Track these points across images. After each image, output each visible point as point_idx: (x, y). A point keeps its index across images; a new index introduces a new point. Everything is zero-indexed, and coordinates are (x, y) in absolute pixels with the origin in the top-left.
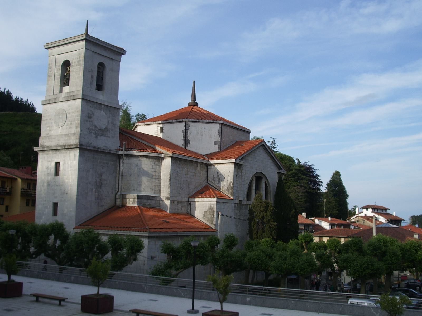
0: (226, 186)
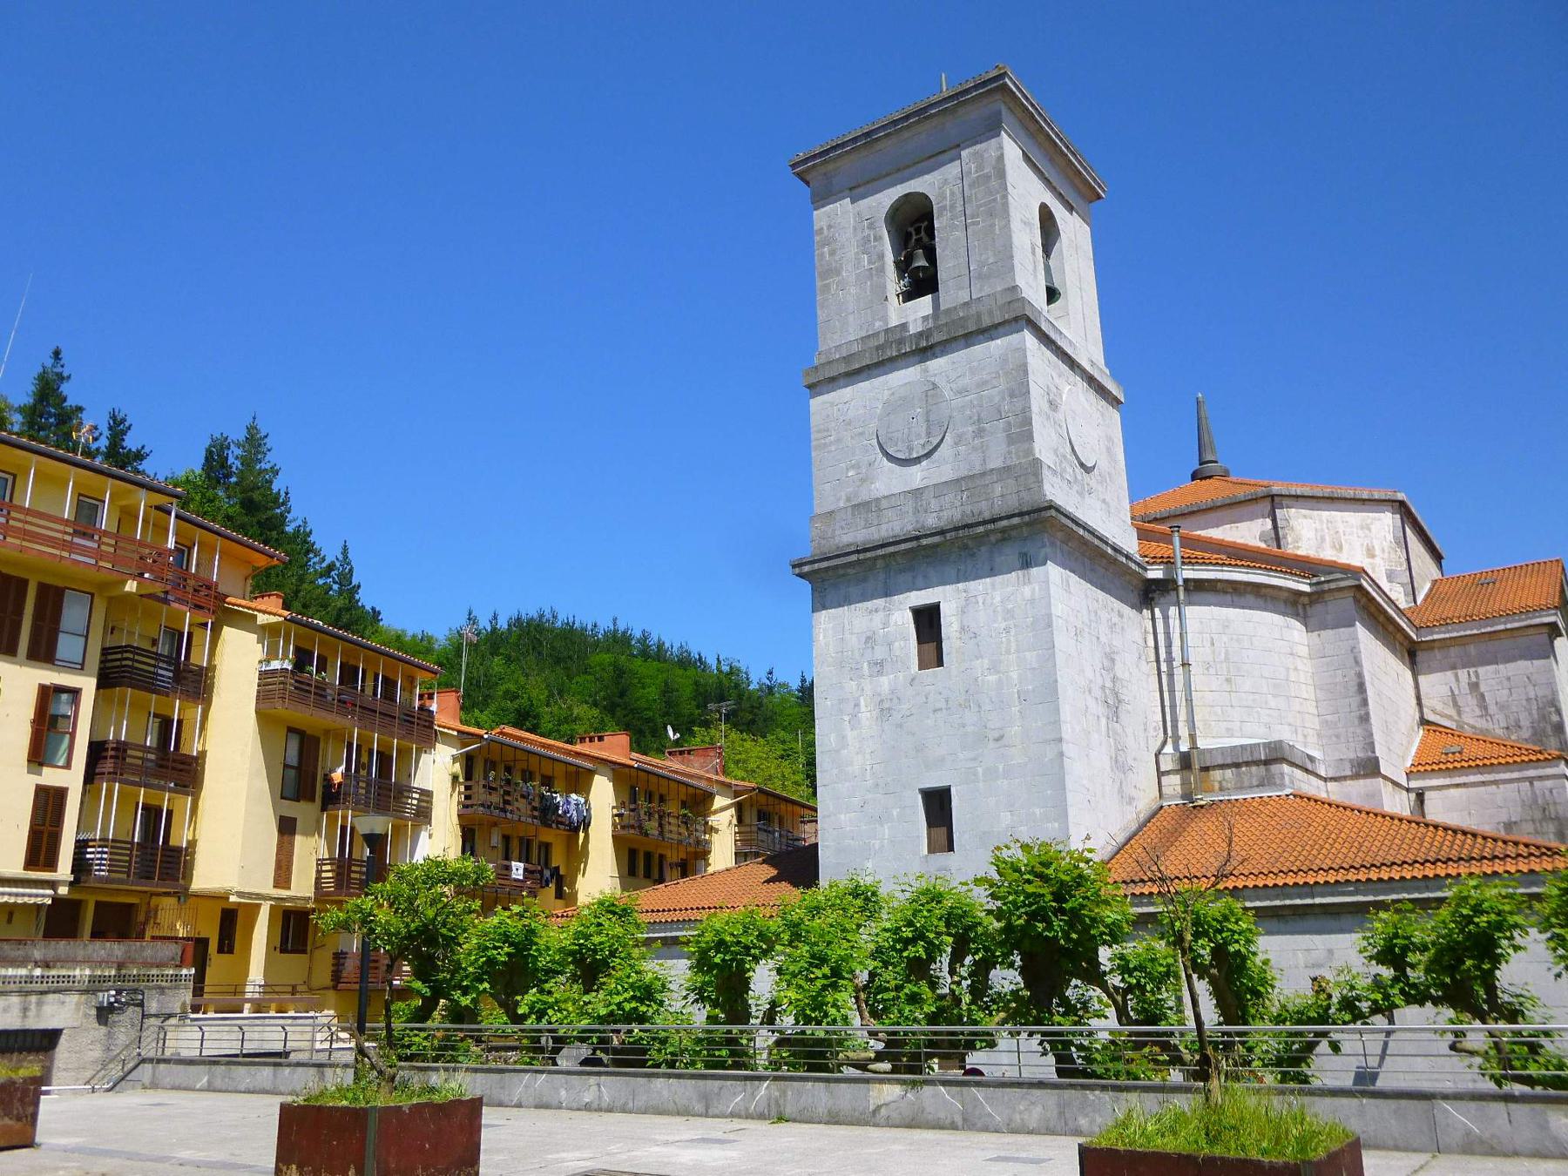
0: (1525, 723)
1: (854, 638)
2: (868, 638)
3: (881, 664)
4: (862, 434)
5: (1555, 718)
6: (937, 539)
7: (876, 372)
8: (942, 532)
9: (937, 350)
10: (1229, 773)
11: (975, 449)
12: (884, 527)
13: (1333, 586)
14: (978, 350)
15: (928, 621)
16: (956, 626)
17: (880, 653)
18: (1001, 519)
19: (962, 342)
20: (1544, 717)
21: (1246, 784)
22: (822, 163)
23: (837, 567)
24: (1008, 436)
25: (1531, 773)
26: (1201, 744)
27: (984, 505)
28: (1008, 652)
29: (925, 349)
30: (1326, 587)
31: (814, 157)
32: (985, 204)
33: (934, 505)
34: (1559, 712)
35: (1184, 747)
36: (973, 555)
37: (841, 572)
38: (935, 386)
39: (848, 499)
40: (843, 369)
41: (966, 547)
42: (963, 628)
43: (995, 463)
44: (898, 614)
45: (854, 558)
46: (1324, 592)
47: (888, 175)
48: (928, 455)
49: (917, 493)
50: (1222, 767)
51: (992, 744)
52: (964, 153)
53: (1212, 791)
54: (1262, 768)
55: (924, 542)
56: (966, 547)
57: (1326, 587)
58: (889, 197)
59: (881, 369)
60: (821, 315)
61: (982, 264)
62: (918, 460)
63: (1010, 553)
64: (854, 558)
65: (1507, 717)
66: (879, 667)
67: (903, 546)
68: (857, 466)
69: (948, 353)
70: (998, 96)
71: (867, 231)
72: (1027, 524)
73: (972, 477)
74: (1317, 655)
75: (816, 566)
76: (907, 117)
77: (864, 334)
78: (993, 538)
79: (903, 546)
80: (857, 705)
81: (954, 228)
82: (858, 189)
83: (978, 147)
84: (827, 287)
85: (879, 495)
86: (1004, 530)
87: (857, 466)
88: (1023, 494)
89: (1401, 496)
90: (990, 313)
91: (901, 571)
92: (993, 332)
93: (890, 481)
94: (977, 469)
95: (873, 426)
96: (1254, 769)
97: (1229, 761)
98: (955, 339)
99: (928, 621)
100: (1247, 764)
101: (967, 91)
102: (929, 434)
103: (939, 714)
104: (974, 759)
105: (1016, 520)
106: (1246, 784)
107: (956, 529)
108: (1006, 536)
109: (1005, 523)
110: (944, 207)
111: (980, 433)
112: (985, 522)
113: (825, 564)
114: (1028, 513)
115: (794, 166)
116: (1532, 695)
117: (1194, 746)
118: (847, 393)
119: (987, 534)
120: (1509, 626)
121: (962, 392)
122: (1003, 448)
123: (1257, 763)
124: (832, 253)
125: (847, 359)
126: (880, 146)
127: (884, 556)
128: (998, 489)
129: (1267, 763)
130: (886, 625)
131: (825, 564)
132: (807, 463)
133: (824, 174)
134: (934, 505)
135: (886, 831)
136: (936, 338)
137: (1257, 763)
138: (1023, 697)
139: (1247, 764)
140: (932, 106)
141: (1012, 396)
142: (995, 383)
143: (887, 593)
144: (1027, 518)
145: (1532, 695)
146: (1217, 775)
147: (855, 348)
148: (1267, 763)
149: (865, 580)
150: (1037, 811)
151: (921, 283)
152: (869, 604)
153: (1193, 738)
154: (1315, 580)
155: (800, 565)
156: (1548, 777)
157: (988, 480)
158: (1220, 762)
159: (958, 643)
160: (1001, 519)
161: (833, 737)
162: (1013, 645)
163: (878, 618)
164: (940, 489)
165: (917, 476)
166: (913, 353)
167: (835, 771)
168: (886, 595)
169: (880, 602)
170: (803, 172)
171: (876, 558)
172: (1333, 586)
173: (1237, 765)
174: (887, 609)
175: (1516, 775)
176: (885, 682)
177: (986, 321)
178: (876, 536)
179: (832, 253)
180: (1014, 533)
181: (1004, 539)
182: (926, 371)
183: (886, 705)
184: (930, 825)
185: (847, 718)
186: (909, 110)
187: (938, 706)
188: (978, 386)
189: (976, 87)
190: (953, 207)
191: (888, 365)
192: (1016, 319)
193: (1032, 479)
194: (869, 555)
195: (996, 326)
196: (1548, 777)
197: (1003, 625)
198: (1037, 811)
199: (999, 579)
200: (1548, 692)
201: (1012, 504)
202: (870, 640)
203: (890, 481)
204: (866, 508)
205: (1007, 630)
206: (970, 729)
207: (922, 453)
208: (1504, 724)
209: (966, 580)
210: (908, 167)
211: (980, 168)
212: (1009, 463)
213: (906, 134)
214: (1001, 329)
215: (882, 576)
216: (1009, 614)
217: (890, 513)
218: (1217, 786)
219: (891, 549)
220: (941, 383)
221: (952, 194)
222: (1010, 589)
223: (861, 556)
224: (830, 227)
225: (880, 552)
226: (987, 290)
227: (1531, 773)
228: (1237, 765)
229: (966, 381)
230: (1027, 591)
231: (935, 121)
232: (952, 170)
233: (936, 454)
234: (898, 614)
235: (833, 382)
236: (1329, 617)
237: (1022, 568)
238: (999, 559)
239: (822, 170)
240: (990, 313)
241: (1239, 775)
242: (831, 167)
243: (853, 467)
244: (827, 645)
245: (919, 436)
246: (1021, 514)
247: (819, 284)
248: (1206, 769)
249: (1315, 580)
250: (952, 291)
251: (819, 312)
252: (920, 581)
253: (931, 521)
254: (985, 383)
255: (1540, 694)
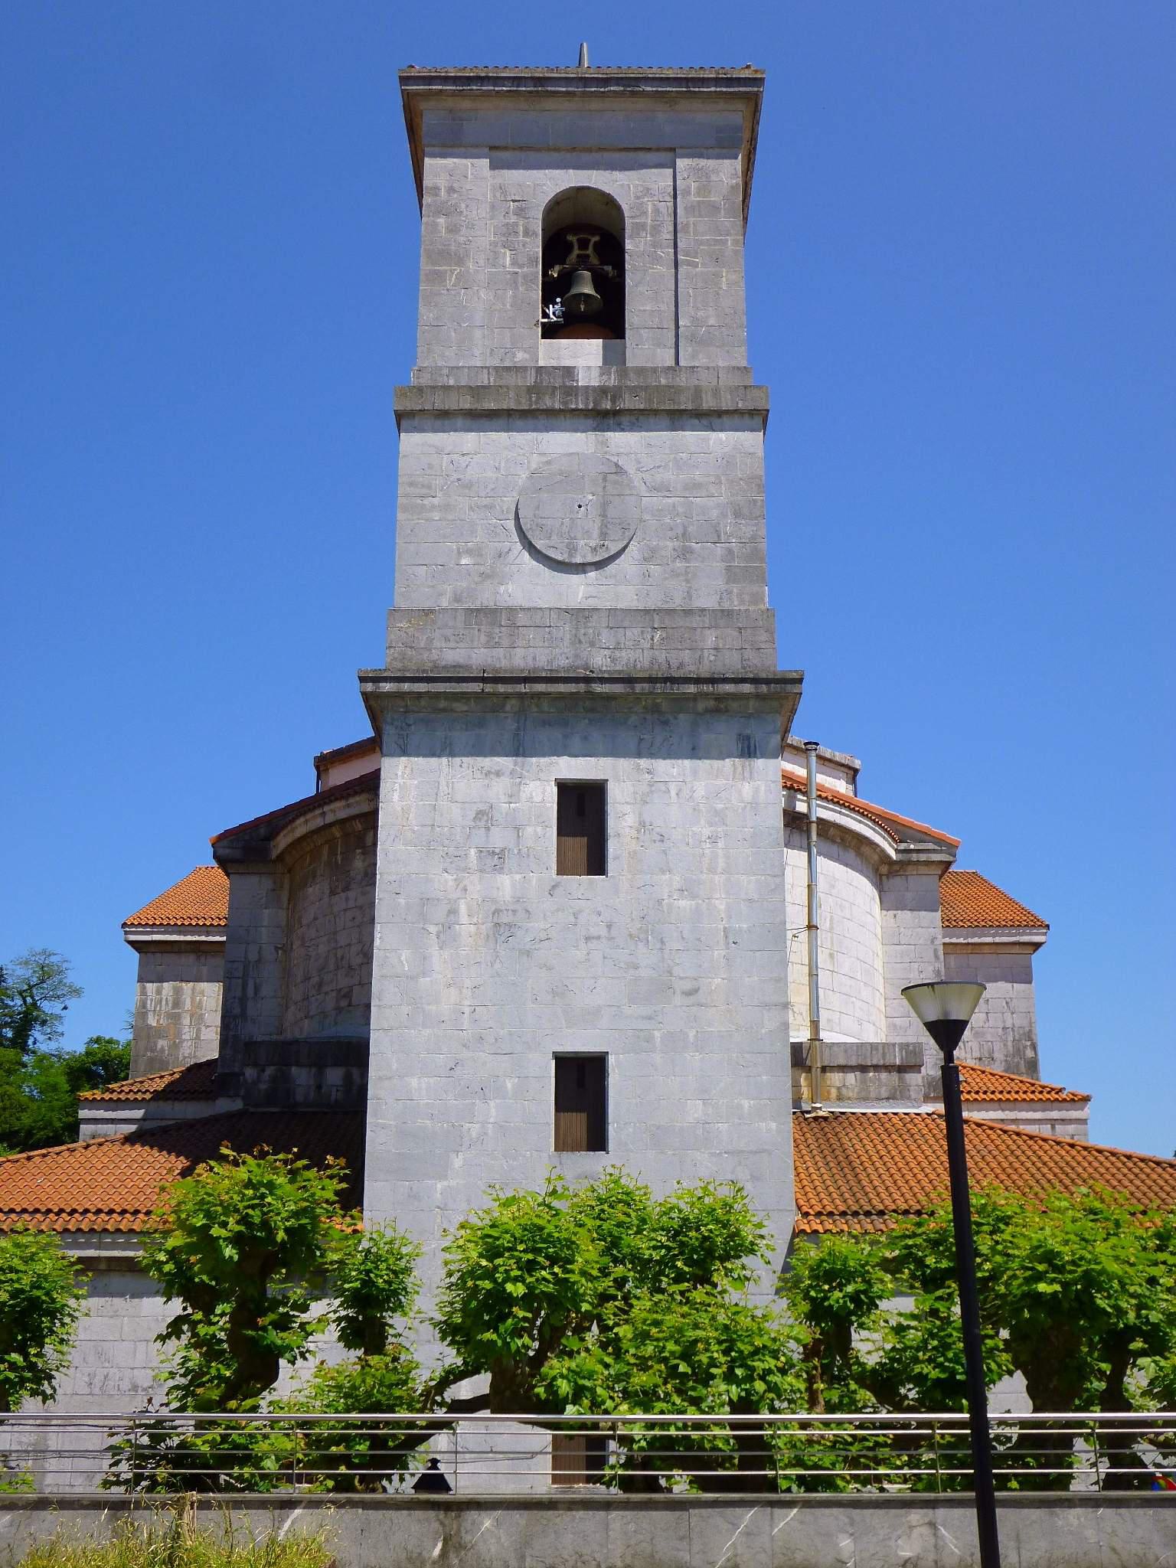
0: (999, 1055)
1: (456, 810)
2: (480, 814)
3: (501, 855)
4: (490, 507)
5: (1030, 1054)
6: (618, 688)
7: (520, 423)
8: (629, 680)
9: (625, 420)
10: (851, 1078)
11: (675, 574)
12: (519, 652)
13: (923, 857)
14: (690, 438)
15: (582, 812)
16: (630, 820)
17: (499, 839)
18: (725, 680)
19: (666, 421)
20: (1019, 1052)
21: (873, 1095)
22: (454, 94)
23: (437, 695)
24: (728, 569)
25: (1055, 1114)
26: (826, 1036)
27: (686, 656)
28: (712, 870)
29: (605, 414)
30: (914, 857)
31: (446, 80)
32: (708, 243)
33: (606, 638)
34: (1034, 1047)
35: (802, 1035)
36: (666, 723)
37: (442, 704)
38: (619, 470)
39: (457, 599)
40: (467, 403)
41: (656, 709)
42: (642, 824)
43: (706, 600)
44: (534, 786)
45: (476, 687)
46: (910, 862)
47: (557, 150)
48: (599, 565)
49: (580, 615)
50: (843, 1068)
51: (678, 1000)
52: (681, 163)
53: (828, 1099)
54: (895, 1076)
55: (598, 688)
56: (656, 709)
57: (914, 857)
58: (549, 183)
59: (531, 422)
60: (426, 314)
61: (696, 322)
62: (581, 568)
63: (724, 731)
64: (476, 687)
65: (981, 1046)
66: (495, 860)
67: (562, 688)
68: (476, 552)
69: (640, 429)
70: (740, 105)
71: (513, 219)
72: (758, 696)
73: (671, 612)
74: (892, 940)
75: (406, 687)
76: (606, 81)
77: (496, 363)
78: (701, 706)
79: (562, 688)
80: (453, 912)
81: (657, 260)
82: (506, 152)
83: (703, 162)
84: (438, 277)
85: (511, 603)
86: (719, 698)
87: (476, 552)
88: (749, 654)
89: (857, 764)
90: (716, 392)
91: (545, 723)
92: (716, 421)
93: (528, 586)
94: (677, 602)
95: (509, 503)
96: (884, 1075)
97: (853, 1063)
98: (656, 412)
99: (582, 812)
100: (876, 1068)
101: (703, 81)
102: (603, 535)
103: (593, 944)
104: (650, 1018)
105: (747, 688)
106: (873, 1095)
107: (652, 680)
108: (721, 706)
109: (729, 688)
110: (643, 226)
111: (684, 554)
112: (698, 681)
113: (422, 687)
114: (767, 681)
115: (404, 80)
116: (1009, 1024)
117: (815, 1038)
118: (469, 440)
119: (695, 697)
120: (997, 940)
121: (663, 489)
122: (720, 583)
123: (888, 1068)
124: (453, 229)
125: (477, 391)
126: (550, 104)
127: (521, 696)
128: (710, 639)
129: (901, 1069)
130: (512, 797)
131: (422, 687)
132: (390, 526)
133: (437, 112)
134: (606, 638)
135: (492, 1110)
136: (627, 403)
137: (888, 1068)
138: (731, 938)
139: (876, 1068)
140: (647, 80)
141: (737, 514)
142: (713, 490)
143: (519, 750)
144: (764, 688)
145: (1009, 1024)
146: (835, 1078)
147: (484, 379)
148: (901, 1069)
149: (481, 724)
150: (746, 1104)
151: (605, 317)
152: (488, 762)
153: (815, 1025)
154: (903, 846)
155: (376, 680)
156: (1070, 1121)
157: (695, 621)
158: (842, 1061)
159: (634, 846)
160: (725, 680)
161: (405, 955)
162: (721, 864)
163: (499, 788)
164: (618, 617)
165: (578, 590)
166: (585, 413)
167: (405, 1009)
168: (516, 754)
169: (505, 762)
170: (417, 94)
171: (507, 696)
172: (923, 857)
173: (863, 1069)
174: (519, 778)
175: (1038, 1115)
176: (505, 885)
177: (708, 403)
178: (504, 664)
179: (453, 229)
180: (734, 705)
181: (716, 711)
182: (605, 443)
183: (505, 919)
184: (560, 1107)
185: (433, 929)
186: (613, 72)
187: (594, 932)
188: (686, 488)
189: (717, 81)
190: (656, 230)
191: (542, 421)
192: (752, 413)
193: (763, 636)
194: (501, 688)
195: (720, 413)
196: (1070, 1121)
197: (707, 831)
198: (746, 1104)
199: (704, 764)
200: (1025, 1023)
201: (730, 663)
202: (484, 816)
203: (528, 586)
204: (492, 618)
205: (713, 840)
206: (644, 973)
207: (590, 559)
208: (977, 1054)
209: (652, 755)
210: (590, 150)
211: (703, 190)
212: (726, 605)
213: (595, 104)
214: (725, 419)
215: (511, 725)
216: (718, 817)
217: (531, 634)
218: (834, 1092)
219: (540, 687)
220: (630, 468)
221: (657, 211)
222: (721, 782)
223: (489, 688)
224: (451, 190)
225: (522, 688)
226: (701, 361)
227: (1055, 1114)
228: (863, 1069)
229: (668, 476)
230: (747, 789)
231: (641, 104)
232: (660, 179)
233: (611, 568)
234: (534, 786)
235: (443, 419)
236: (909, 895)
237: (742, 756)
238: (705, 737)
239: (450, 103)
240: (716, 392)
241: (864, 1082)
242: (466, 104)
243: (469, 552)
244: (405, 811)
245: (587, 534)
246: (755, 681)
247: (425, 266)
248: (824, 1069)
249: (903, 846)
250: (646, 342)
251: (422, 309)
252: (576, 742)
253: (600, 661)
254: (698, 486)
255: (1018, 1023)
